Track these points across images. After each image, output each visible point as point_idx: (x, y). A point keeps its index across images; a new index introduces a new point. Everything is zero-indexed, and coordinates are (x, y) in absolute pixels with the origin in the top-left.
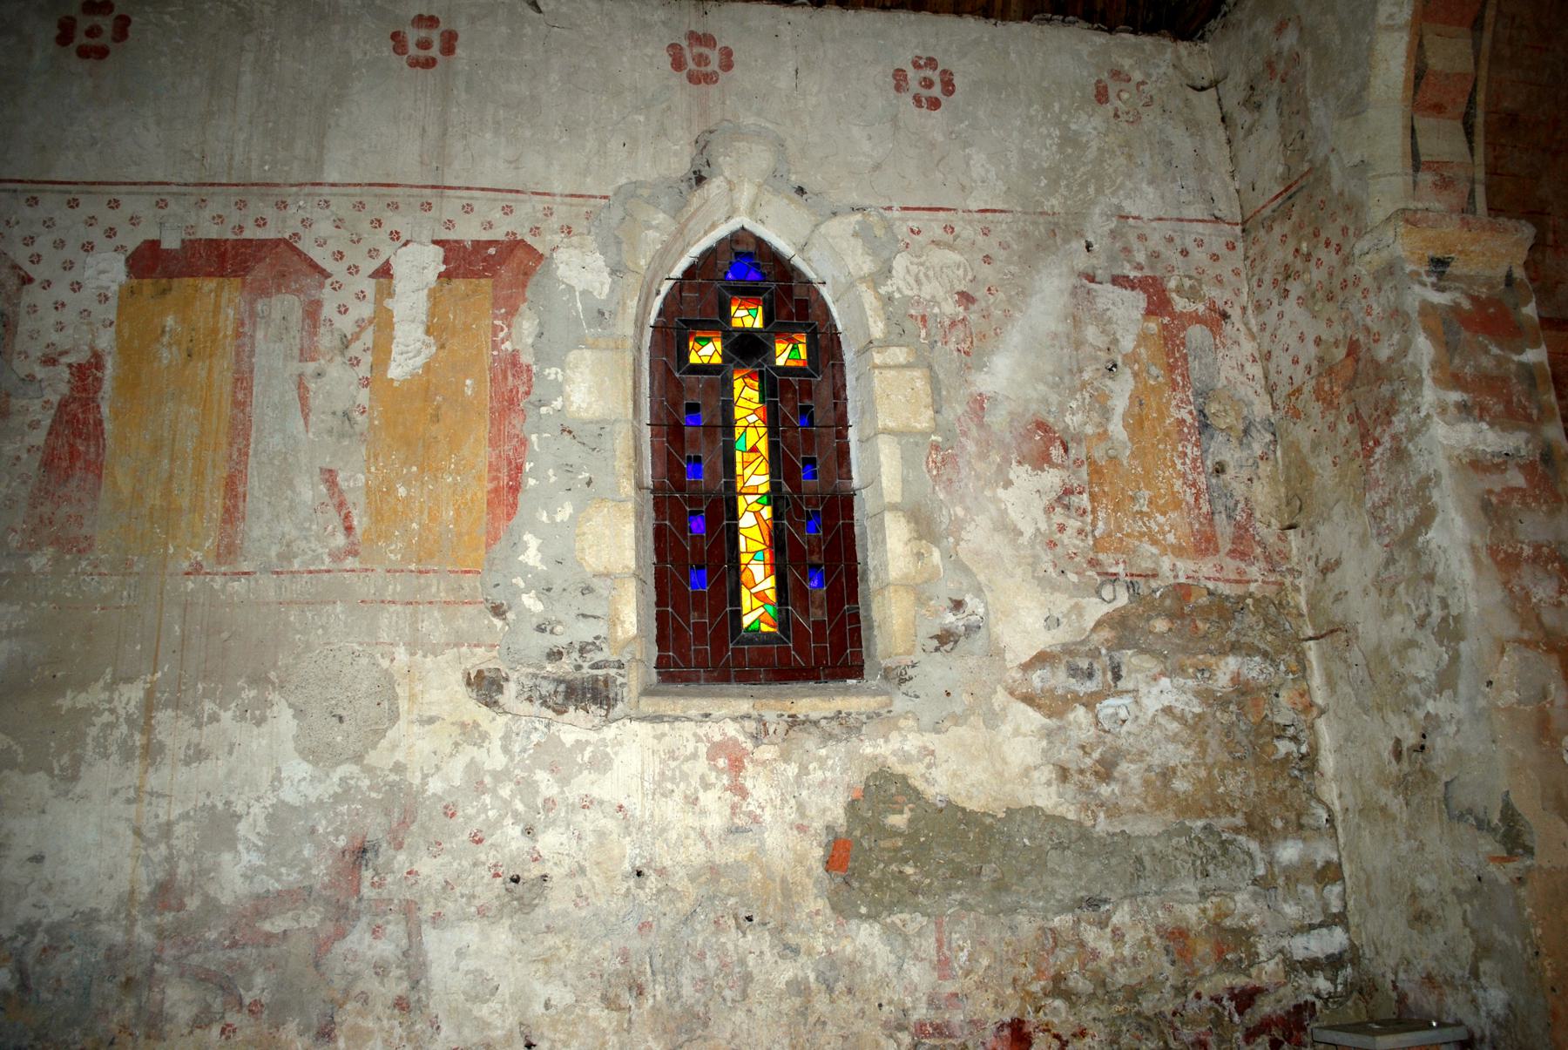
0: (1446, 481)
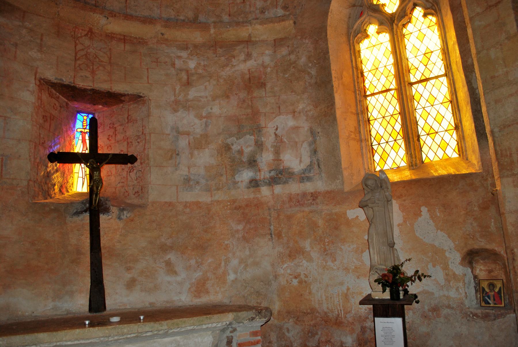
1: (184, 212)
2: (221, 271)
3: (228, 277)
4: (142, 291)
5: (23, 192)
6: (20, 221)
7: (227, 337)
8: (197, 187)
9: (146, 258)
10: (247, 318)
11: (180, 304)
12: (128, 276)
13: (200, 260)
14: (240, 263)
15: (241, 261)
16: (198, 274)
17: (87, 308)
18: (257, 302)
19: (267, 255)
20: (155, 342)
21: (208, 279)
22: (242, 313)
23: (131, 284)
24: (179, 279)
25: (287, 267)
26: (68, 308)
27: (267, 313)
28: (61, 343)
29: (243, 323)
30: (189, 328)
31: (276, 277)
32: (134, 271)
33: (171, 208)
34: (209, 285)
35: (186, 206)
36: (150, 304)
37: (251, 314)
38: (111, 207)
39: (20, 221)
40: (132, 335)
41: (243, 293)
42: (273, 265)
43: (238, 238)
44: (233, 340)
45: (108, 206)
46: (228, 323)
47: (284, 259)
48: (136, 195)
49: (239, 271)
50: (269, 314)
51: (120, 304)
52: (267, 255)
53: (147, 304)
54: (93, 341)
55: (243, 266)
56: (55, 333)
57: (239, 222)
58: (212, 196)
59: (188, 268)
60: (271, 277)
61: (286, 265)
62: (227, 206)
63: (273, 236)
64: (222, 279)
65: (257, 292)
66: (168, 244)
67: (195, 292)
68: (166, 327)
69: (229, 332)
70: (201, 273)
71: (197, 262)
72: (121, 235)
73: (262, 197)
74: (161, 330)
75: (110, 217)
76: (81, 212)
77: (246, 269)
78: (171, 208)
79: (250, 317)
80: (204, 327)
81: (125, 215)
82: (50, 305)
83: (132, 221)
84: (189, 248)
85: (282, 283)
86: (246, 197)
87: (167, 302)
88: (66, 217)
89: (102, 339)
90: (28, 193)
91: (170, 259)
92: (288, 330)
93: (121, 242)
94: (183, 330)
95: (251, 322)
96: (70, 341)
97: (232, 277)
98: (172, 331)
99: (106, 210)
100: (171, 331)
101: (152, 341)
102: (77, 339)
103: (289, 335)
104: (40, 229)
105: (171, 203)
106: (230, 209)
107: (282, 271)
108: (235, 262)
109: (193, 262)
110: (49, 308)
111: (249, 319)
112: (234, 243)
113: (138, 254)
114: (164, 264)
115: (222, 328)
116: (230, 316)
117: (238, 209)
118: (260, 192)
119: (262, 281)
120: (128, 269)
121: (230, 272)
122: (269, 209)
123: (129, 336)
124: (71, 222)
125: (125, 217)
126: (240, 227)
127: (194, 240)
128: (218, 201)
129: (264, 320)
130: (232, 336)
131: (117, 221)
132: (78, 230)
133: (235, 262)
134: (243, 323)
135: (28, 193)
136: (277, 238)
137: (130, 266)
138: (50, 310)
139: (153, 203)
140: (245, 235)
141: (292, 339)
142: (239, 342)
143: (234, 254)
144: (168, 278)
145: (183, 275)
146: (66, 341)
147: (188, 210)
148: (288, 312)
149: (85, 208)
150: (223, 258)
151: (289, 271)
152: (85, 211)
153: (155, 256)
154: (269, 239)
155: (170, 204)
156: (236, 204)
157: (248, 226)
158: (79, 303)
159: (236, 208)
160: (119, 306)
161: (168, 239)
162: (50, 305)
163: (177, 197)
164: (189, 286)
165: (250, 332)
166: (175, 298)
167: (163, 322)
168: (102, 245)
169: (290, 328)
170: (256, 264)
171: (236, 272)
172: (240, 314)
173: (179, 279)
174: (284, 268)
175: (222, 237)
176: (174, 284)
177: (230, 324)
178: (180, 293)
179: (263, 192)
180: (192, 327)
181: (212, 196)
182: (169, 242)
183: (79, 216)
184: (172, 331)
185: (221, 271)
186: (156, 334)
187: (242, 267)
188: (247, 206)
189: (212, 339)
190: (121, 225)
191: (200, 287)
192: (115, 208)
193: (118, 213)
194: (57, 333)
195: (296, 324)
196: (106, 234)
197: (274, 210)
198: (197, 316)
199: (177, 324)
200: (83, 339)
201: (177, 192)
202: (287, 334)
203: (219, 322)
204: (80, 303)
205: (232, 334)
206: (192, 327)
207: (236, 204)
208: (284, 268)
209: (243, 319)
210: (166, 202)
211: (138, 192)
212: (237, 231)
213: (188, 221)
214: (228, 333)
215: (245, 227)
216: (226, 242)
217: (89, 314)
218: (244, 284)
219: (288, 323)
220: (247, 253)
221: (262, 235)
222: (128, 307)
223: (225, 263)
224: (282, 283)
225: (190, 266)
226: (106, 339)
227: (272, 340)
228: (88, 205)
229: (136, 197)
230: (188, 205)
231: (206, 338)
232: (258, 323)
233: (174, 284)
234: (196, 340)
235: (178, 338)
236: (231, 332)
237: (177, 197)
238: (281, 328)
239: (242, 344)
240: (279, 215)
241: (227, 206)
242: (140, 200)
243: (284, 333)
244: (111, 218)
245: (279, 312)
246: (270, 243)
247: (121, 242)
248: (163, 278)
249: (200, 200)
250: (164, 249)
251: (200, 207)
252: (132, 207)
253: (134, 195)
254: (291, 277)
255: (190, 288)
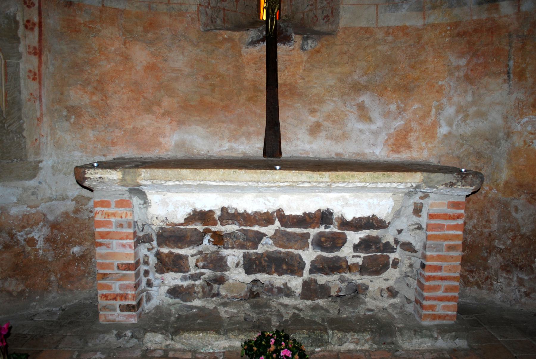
0: (235, 145)
1: (385, 40)
2: (429, 121)
3: (438, 130)
4: (327, 138)
5: (192, 19)
6: (191, 51)
7: (415, 203)
8: (404, 6)
9: (334, 99)
10: (444, 183)
11: (373, 158)
12: (312, 119)
13: (402, 105)
14: (458, 112)
15: (460, 109)
16: (399, 123)
17: (262, 152)
18: (476, 167)
19: (498, 104)
20: (317, 196)
21: (411, 130)
22: (436, 174)
23: (315, 130)
24: (374, 127)
25: (527, 122)
26: (244, 151)
27: (474, 180)
28: (205, 182)
29: (437, 188)
30: (359, 185)
31: (508, 135)
32: (318, 114)
33: (367, 35)
34: (412, 138)
35: (387, 33)
36: (337, 154)
37: (450, 178)
38: (293, 35)
39: (191, 51)
40: (286, 184)
41: (457, 152)
42: (505, 118)
43: (459, 78)
44: (423, 209)
45: (288, 34)
46: (414, 185)
47: (525, 111)
48: (325, 20)
49: (456, 123)
50: (478, 182)
51: (301, 152)
52: (498, 104)
53: (333, 155)
54: (239, 184)
55: (461, 116)
56: (198, 171)
57: (462, 55)
58: (424, 18)
59: (386, 115)
60: (501, 135)
61: (526, 119)
62: (446, 32)
63: (512, 76)
64: (430, 132)
65: (478, 153)
66: (362, 82)
67: (394, 145)
68: (328, 180)
69: (418, 198)
70: (403, 123)
71: (398, 107)
72: (304, 70)
73: (500, 17)
74: (322, 182)
75: (292, 47)
76: (258, 42)
77: (465, 121)
78: (367, 35)
79: (447, 182)
80: (380, 185)
81: (310, 45)
82: (226, 145)
83: (318, 52)
84: (389, 89)
85: (517, 145)
86: (475, 18)
87: (358, 154)
88: (241, 48)
89: (250, 183)
90: (199, 20)
91: (363, 101)
92: (516, 210)
93: (304, 79)
94: (351, 186)
95: (450, 189)
96: (214, 181)
97: (444, 130)
98: (336, 185)
99: (287, 39)
100: (334, 185)
101: (313, 194)
102: (221, 180)
103: (518, 216)
104: (213, 61)
105: (368, 28)
106: (450, 36)
107: (519, 128)
108: (450, 111)
109: (393, 107)
110: (225, 149)
111: (446, 185)
112: (451, 84)
113: (324, 94)
114: (356, 108)
115: (406, 191)
116: (418, 177)
117: (462, 36)
118: (497, 9)
119: (487, 140)
120: (313, 112)
121: (443, 123)
122: (510, 35)
123: (281, 184)
124: (247, 53)
125: (309, 48)
126: (462, 62)
127: (396, 79)
128: (433, 25)
129: (469, 189)
130: (422, 204)
131: (301, 52)
132: (255, 63)
133: (450, 111)
134: (437, 188)
135: (199, 20)
136: (516, 80)
137: (314, 108)
138: (225, 151)
139: (346, 28)
140: (469, 73)
141: (521, 222)
142: (431, 212)
143: (450, 99)
144: (360, 126)
145: (379, 123)
146: (210, 180)
147: (390, 38)
148: (521, 185)
149: (262, 37)
150: (435, 103)
151: (529, 128)
152: (263, 41)
153: (346, 97)
154: (505, 80)
155: (367, 30)
156: (459, 29)
157: (475, 60)
158: (257, 146)
159: (459, 35)
160: (301, 153)
161: (363, 76)
162: (226, 145)
163: (377, 20)
164: (386, 138)
165: (449, 202)
166: (368, 151)
167: (324, 173)
168: (280, 81)
169: (520, 207)
170: (481, 115)
171: (450, 124)
172: (433, 175)
173: (374, 127)
174: (522, 123)
175: (435, 75)
176: (367, 134)
177: (418, 187)
178: (373, 145)
179: (502, 10)
180: (362, 184)
181: (424, 18)
182: (363, 80)
183: (255, 46)
184: (336, 185)
185: (429, 121)
186: (316, 186)
187: (460, 118)
188: (475, 31)
189: (393, 203)
190: (305, 58)
191: (400, 140)
192: (298, 36)
193: (301, 42)
194: (200, 170)
195: (530, 202)
196: (286, 68)
197: (518, 36)
198: (371, 171)
199: (343, 178)
200: (229, 181)
201: (377, 13)
202: (514, 214)
203: (402, 183)
204: (255, 147)
205: (421, 201)
206: (362, 184)
207: (459, 29)
208: (522, 123)
209: (438, 182)
210: (362, 28)
211: (327, 16)
212: (458, 68)
213: (389, 53)
214: (416, 199)
215: (469, 62)
216: (440, 83)
217: (263, 158)
218: (461, 141)
219: (518, 200)
220: (469, 98)
221: (494, 73)
222: (311, 155)
223: (437, 111)
224: (517, 145)
225: (389, 113)
226: (255, 184)
227: (491, 218)
228: (264, 33)
229: (326, 22)
230: (391, 31)
231: (384, 201)
232: (460, 192)
233: (367, 134)
234: (371, 201)
235: (347, 195)
236: (421, 198)
237: (377, 20)
238: (506, 205)
239: (435, 215)
240: (524, 45)
241: (446, 32)
242: (330, 27)
243: (509, 212)
244: (293, 49)
245: (506, 183)
246: (506, 86)
247: (304, 79)
248: (354, 124)
249: (408, 24)
250: (357, 88)
251: (407, 34)
252: (320, 34)
253: (324, 19)
254: (531, 136)
255: (387, 140)
